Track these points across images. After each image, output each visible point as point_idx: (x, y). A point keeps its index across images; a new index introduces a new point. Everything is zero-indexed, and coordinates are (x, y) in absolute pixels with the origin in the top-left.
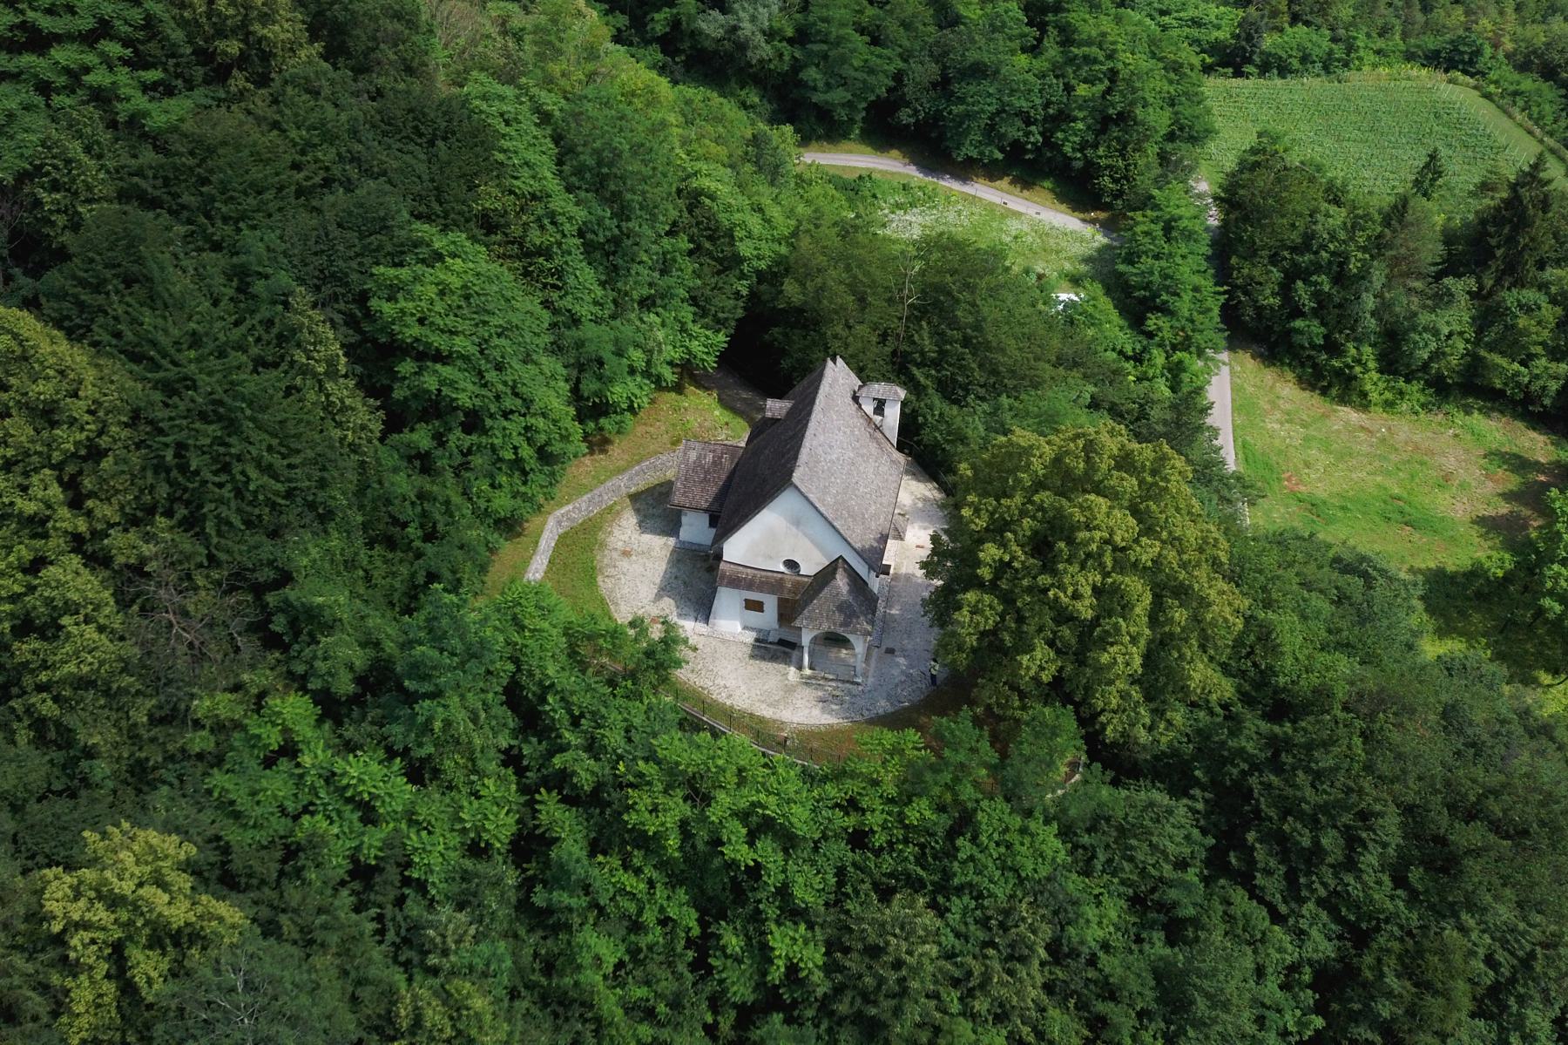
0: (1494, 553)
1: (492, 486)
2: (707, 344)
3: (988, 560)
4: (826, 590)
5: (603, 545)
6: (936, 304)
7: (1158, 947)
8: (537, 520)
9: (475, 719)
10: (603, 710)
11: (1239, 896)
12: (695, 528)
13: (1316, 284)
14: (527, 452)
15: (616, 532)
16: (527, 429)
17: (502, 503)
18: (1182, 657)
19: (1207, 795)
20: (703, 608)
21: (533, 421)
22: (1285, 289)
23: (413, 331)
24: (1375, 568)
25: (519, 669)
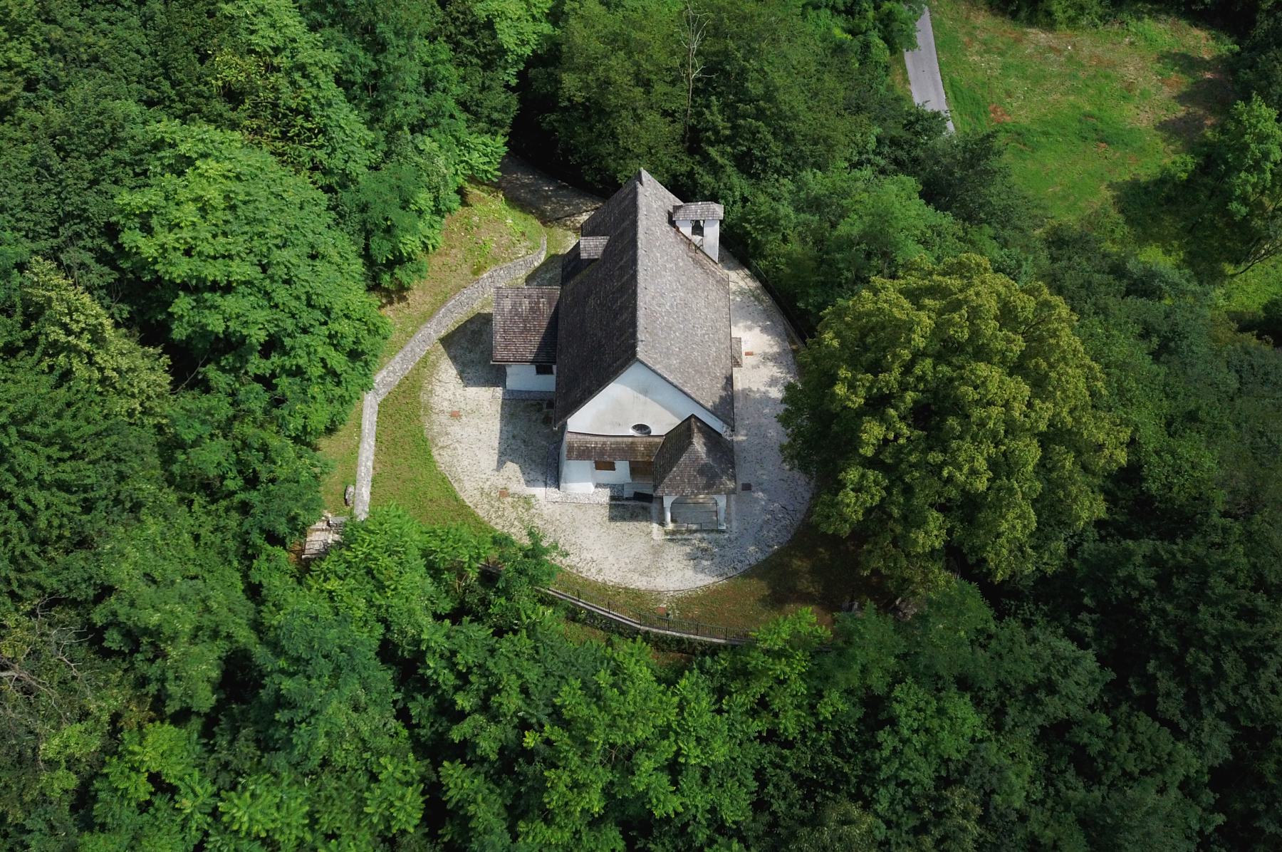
0: (1177, 158)
2: (488, 150)
5: (428, 408)
7: (1077, 792)
11: (1143, 722)
15: (438, 390)
16: (330, 336)
18: (1068, 495)
19: (1095, 616)
23: (181, 269)
24: (1167, 283)
25: (388, 628)
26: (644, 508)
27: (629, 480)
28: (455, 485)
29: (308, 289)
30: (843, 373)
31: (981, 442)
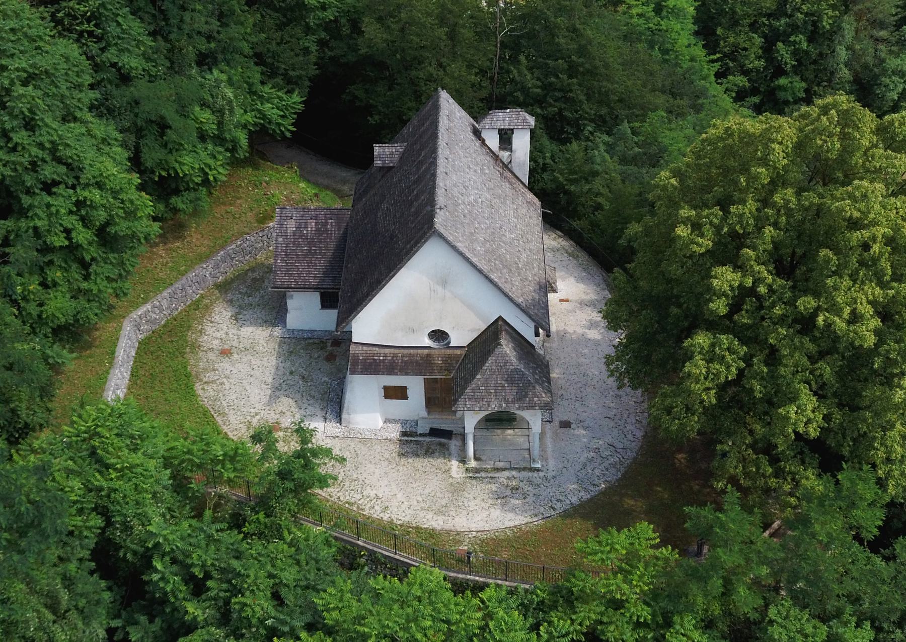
1: (44, 285)
2: (281, 107)
3: (726, 288)
4: (491, 360)
5: (195, 347)
6: (531, 36)
8: (111, 326)
9: (53, 605)
10: (235, 563)
12: (305, 312)
13: (795, 42)
14: (82, 236)
15: (209, 330)
17: (59, 305)
20: (334, 404)
21: (86, 193)
22: (768, 50)
25: (109, 523)
26: (442, 445)
27: (424, 413)
28: (219, 419)
29: (55, 138)
30: (685, 212)
31: (863, 283)
